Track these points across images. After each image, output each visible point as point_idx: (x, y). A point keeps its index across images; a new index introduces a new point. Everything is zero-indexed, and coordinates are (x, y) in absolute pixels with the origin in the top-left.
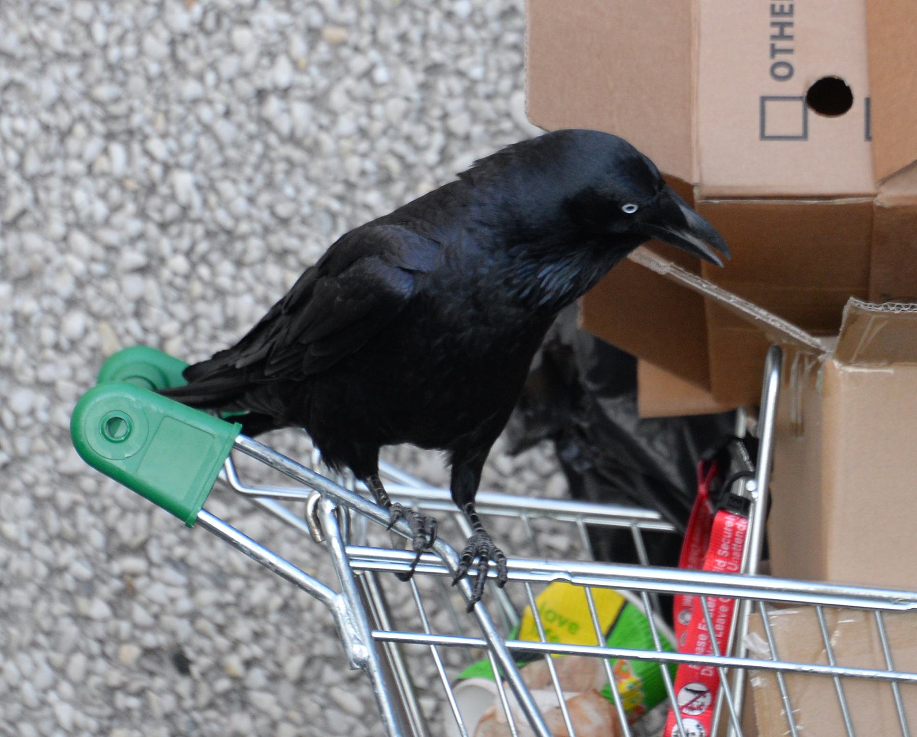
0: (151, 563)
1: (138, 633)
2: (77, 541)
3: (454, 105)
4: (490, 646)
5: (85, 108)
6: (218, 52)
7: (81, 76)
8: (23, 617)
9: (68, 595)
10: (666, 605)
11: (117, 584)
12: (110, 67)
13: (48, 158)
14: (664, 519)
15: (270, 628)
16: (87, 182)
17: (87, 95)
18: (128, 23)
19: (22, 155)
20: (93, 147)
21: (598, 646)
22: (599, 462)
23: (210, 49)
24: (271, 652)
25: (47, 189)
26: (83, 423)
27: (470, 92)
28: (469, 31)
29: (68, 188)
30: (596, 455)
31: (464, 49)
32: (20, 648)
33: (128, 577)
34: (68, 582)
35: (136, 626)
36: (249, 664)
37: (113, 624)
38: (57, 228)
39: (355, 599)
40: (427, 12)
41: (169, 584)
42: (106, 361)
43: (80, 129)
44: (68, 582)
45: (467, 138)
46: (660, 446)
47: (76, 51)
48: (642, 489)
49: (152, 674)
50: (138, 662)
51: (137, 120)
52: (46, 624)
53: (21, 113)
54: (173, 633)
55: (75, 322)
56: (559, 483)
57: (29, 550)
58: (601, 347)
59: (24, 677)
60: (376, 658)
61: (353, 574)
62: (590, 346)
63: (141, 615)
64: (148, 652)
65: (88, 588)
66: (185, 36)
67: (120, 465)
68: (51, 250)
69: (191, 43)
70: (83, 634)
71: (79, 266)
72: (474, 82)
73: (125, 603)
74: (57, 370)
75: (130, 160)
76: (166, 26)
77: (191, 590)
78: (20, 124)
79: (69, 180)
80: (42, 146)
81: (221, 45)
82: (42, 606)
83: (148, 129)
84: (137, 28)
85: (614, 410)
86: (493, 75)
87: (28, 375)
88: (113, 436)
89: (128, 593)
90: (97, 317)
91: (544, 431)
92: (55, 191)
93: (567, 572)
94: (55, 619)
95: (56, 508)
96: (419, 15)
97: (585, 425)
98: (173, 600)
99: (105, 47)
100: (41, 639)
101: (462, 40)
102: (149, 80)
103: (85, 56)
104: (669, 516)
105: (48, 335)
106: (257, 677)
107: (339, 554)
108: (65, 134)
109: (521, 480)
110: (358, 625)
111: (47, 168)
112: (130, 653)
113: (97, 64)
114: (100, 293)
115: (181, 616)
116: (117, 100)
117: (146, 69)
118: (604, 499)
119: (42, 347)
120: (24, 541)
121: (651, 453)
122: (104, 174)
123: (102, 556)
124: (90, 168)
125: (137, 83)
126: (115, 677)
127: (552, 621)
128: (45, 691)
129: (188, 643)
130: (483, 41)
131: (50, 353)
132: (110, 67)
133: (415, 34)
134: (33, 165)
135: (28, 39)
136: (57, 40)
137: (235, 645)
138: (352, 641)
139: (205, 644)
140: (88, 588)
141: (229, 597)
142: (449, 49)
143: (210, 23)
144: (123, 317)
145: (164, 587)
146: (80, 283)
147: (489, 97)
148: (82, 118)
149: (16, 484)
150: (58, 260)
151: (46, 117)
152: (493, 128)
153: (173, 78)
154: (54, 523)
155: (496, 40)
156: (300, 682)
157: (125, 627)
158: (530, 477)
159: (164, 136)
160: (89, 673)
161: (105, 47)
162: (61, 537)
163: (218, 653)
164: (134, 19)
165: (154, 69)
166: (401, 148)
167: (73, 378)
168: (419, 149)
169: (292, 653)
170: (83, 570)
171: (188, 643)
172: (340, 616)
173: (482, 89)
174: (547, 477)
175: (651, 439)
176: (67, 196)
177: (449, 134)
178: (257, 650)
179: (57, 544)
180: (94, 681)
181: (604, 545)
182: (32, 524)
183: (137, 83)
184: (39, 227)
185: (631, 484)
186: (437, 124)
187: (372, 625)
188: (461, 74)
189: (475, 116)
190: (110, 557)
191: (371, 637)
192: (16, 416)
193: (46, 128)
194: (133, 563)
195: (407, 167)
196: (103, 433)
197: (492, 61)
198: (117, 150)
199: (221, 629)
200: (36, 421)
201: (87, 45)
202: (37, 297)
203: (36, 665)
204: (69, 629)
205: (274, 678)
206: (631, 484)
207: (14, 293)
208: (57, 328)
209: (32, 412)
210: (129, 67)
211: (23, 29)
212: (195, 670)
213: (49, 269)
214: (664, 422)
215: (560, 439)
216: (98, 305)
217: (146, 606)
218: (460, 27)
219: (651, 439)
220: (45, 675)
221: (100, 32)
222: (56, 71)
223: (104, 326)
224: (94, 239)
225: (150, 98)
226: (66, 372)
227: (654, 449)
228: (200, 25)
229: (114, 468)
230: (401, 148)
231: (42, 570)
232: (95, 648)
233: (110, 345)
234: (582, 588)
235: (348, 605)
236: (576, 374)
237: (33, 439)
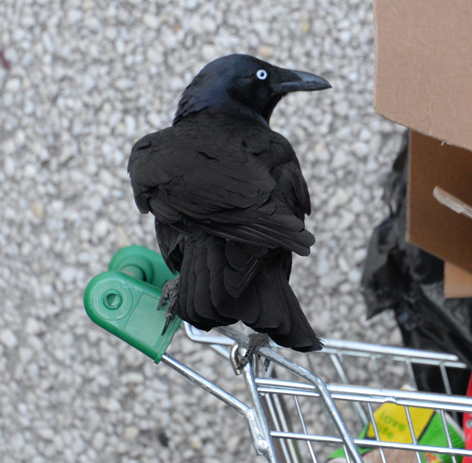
0: (146, 378)
1: (137, 421)
2: (101, 362)
3: (339, 97)
4: (344, 442)
5: (111, 93)
6: (193, 61)
7: (109, 73)
8: (66, 408)
9: (94, 396)
10: (460, 417)
11: (124, 390)
12: (127, 69)
13: (87, 124)
14: (460, 360)
15: (218, 420)
16: (111, 139)
17: (112, 86)
18: (138, 41)
19: (71, 122)
20: (115, 118)
21: (413, 444)
22: (421, 323)
23: (189, 58)
24: (218, 434)
25: (87, 144)
26: (91, 297)
27: (348, 89)
28: (349, 51)
29: (99, 143)
30: (419, 319)
31: (346, 62)
32: (65, 428)
33: (131, 385)
34: (94, 387)
35: (135, 416)
36: (205, 441)
37: (121, 415)
38: (92, 167)
39: (260, 411)
40: (323, 39)
41: (156, 391)
42: (121, 250)
43: (107, 107)
44: (94, 387)
45: (346, 118)
46: (458, 315)
47: (105, 58)
48: (447, 341)
49: (145, 446)
50: (137, 438)
51: (142, 102)
52: (80, 413)
53: (70, 96)
54: (158, 421)
55: (102, 227)
56: (397, 336)
57: (70, 367)
58: (423, 254)
59: (66, 446)
60: (273, 448)
61: (260, 395)
62: (416, 253)
63: (139, 409)
64: (143, 432)
65: (106, 392)
66: (173, 50)
67: (114, 323)
68: (88, 181)
69: (177, 55)
70: (103, 420)
71: (105, 192)
72: (351, 83)
73: (130, 402)
74: (91, 256)
75: (137, 127)
76: (162, 43)
77: (170, 395)
78: (71, 103)
79: (100, 138)
80: (83, 117)
81: (195, 56)
82: (78, 402)
83: (149, 108)
84: (143, 44)
85: (430, 292)
86: (363, 79)
87: (72, 259)
88: (110, 305)
89: (131, 395)
90: (116, 224)
91: (387, 303)
92: (91, 145)
93: (393, 397)
94: (86, 410)
95: (88, 341)
96: (318, 40)
97: (412, 301)
98: (159, 401)
99: (124, 56)
100: (78, 423)
101: (344, 57)
102: (151, 77)
103: (111, 62)
104: (463, 357)
105: (85, 234)
106: (210, 449)
107: (251, 383)
108: (98, 110)
109: (375, 331)
110: (262, 428)
111: (86, 130)
112: (132, 432)
113: (118, 67)
114: (118, 209)
115: (164, 410)
116: (130, 89)
117: (148, 71)
118: (423, 347)
119: (81, 242)
120: (68, 362)
121: (453, 320)
122: (122, 135)
123: (116, 372)
124: (113, 132)
125: (143, 78)
126: (122, 448)
127: (389, 422)
128: (79, 455)
129: (168, 427)
130: (357, 57)
131: (86, 246)
132: (127, 69)
133: (315, 52)
134: (78, 128)
135: (76, 50)
136: (94, 51)
137: (197, 430)
138: (258, 437)
139: (178, 428)
140: (106, 392)
141: (193, 400)
142: (337, 62)
143: (189, 42)
144: (131, 224)
145: (154, 393)
146: (106, 202)
147: (361, 92)
148: (108, 100)
149: (64, 326)
150: (92, 187)
151: (87, 99)
152: (363, 112)
153: (166, 76)
154: (87, 351)
155: (366, 57)
156: (236, 453)
157: (129, 417)
158: (380, 329)
159: (159, 112)
160: (106, 444)
161: (124, 56)
162: (91, 360)
163: (186, 435)
164: (142, 38)
165: (154, 70)
166: (305, 123)
167: (100, 261)
168: (316, 124)
169: (231, 435)
170: (104, 381)
171: (168, 427)
172: (250, 421)
173: (356, 87)
174: (391, 330)
175: (453, 311)
176: (98, 148)
177: (335, 115)
178: (209, 433)
179: (88, 364)
180: (109, 449)
181: (423, 376)
182: (72, 351)
183: (143, 78)
184: (81, 167)
185: (442, 339)
186: (328, 108)
187: (271, 427)
188: (343, 78)
189: (351, 104)
190: (121, 373)
191: (270, 435)
192: (65, 284)
193: (86, 106)
194: (135, 377)
195: (309, 135)
196: (104, 303)
197: (363, 70)
198: (130, 120)
199: (188, 419)
200: (77, 288)
201: (112, 55)
202: (80, 210)
203: (74, 439)
204: (95, 417)
205: (221, 450)
206: (442, 339)
207: (65, 208)
208: (91, 229)
209: (74, 282)
210: (138, 68)
211: (74, 43)
212: (172, 444)
213: (87, 193)
214: (462, 301)
215: (397, 308)
216: (116, 216)
217: (143, 403)
218: (343, 48)
219: (453, 311)
220: (79, 445)
221: (121, 47)
222: (94, 70)
223: (120, 230)
224: (114, 175)
225: (151, 88)
226: (96, 257)
227: (454, 316)
228: (183, 44)
229: (111, 326)
230: (305, 123)
231: (79, 380)
232: (110, 429)
233: (123, 241)
234: (403, 407)
235: (256, 415)
236: (408, 269)
237: (75, 298)
